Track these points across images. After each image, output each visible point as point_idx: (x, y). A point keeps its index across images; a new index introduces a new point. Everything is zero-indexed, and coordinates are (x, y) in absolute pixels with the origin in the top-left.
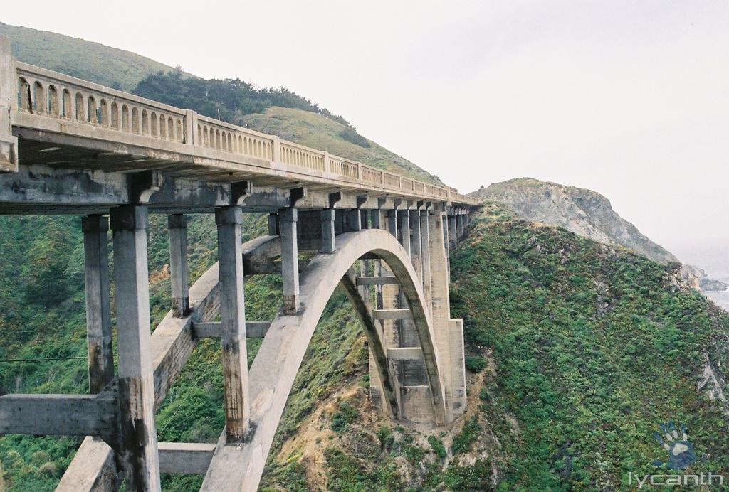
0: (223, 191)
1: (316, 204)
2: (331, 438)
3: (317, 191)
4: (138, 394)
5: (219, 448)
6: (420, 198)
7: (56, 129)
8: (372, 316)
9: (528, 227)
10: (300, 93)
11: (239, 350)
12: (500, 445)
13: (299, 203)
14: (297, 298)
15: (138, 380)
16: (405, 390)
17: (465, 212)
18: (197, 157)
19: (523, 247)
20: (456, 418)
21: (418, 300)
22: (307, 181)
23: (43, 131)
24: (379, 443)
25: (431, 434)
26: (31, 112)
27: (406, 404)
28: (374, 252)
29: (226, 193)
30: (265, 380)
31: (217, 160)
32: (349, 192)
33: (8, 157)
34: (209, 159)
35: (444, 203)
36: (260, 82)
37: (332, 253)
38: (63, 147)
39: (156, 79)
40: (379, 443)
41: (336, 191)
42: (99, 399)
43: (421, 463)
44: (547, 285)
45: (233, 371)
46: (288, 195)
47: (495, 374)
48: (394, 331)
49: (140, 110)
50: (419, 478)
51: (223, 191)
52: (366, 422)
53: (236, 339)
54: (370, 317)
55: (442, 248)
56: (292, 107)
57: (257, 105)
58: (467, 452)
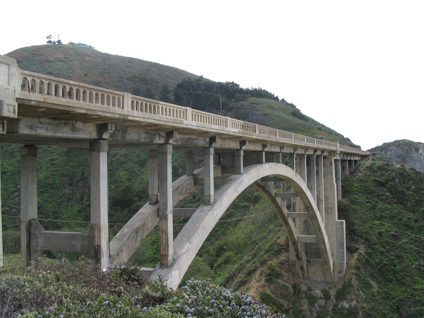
2: (264, 286)
4: (99, 232)
5: (156, 270)
7: (42, 100)
9: (392, 168)
10: (269, 90)
12: (364, 297)
16: (310, 261)
17: (357, 158)
19: (387, 179)
20: (339, 279)
21: (311, 207)
22: (212, 132)
23: (35, 101)
24: (292, 291)
25: (323, 288)
26: (29, 93)
27: (310, 270)
30: (186, 238)
31: (144, 118)
32: (255, 141)
33: (12, 111)
34: (139, 117)
35: (334, 152)
36: (245, 85)
37: (241, 174)
38: (48, 109)
39: (187, 82)
40: (292, 291)
42: (82, 234)
43: (316, 305)
44: (401, 203)
45: (164, 230)
46: (208, 140)
47: (364, 254)
48: (304, 226)
49: (94, 93)
50: (314, 313)
51: (160, 136)
52: (285, 278)
53: (166, 213)
54: (285, 216)
56: (263, 97)
57: (243, 97)
58: (344, 299)
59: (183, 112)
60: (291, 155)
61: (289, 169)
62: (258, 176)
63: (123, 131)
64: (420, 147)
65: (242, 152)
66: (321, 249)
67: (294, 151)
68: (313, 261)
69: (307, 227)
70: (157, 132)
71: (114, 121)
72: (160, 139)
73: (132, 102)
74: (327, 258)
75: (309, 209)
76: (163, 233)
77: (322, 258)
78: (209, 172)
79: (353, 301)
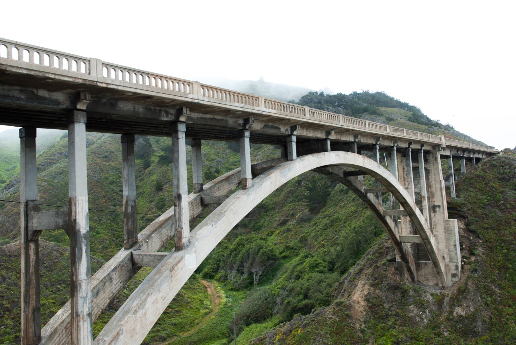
35: (439, 145)
59: (303, 110)
60: (406, 149)
61: (373, 162)
65: (294, 139)
67: (422, 147)
70: (163, 109)
77: (430, 260)
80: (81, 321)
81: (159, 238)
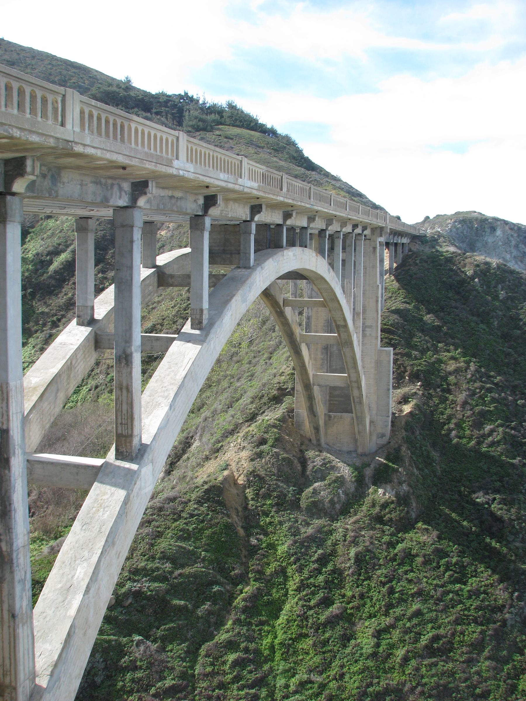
0: (121, 189)
1: (234, 215)
3: (235, 200)
6: (354, 220)
8: (298, 339)
11: (131, 363)
13: (214, 211)
14: (205, 312)
15: (4, 387)
16: (330, 417)
17: (405, 240)
18: (76, 143)
21: (346, 326)
22: (218, 186)
24: (299, 468)
28: (299, 272)
29: (125, 192)
31: (103, 149)
32: (274, 206)
35: (382, 229)
37: (249, 268)
41: (257, 202)
45: (124, 384)
46: (201, 201)
51: (121, 189)
53: (128, 352)
54: (297, 341)
55: (376, 274)
62: (277, 273)
63: (53, 176)
64: (497, 226)
66: (353, 398)
68: (335, 417)
69: (327, 358)
70: (115, 182)
71: (39, 154)
72: (120, 198)
73: (82, 112)
74: (362, 412)
75: (342, 329)
76: (122, 392)
78: (202, 265)
79: (402, 485)
80: (21, 625)
81: (39, 420)
